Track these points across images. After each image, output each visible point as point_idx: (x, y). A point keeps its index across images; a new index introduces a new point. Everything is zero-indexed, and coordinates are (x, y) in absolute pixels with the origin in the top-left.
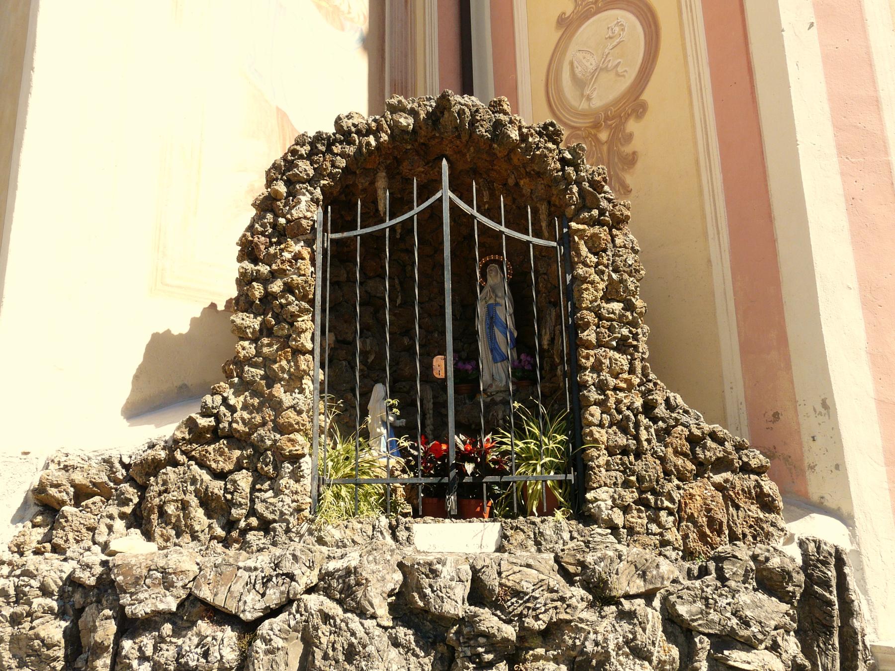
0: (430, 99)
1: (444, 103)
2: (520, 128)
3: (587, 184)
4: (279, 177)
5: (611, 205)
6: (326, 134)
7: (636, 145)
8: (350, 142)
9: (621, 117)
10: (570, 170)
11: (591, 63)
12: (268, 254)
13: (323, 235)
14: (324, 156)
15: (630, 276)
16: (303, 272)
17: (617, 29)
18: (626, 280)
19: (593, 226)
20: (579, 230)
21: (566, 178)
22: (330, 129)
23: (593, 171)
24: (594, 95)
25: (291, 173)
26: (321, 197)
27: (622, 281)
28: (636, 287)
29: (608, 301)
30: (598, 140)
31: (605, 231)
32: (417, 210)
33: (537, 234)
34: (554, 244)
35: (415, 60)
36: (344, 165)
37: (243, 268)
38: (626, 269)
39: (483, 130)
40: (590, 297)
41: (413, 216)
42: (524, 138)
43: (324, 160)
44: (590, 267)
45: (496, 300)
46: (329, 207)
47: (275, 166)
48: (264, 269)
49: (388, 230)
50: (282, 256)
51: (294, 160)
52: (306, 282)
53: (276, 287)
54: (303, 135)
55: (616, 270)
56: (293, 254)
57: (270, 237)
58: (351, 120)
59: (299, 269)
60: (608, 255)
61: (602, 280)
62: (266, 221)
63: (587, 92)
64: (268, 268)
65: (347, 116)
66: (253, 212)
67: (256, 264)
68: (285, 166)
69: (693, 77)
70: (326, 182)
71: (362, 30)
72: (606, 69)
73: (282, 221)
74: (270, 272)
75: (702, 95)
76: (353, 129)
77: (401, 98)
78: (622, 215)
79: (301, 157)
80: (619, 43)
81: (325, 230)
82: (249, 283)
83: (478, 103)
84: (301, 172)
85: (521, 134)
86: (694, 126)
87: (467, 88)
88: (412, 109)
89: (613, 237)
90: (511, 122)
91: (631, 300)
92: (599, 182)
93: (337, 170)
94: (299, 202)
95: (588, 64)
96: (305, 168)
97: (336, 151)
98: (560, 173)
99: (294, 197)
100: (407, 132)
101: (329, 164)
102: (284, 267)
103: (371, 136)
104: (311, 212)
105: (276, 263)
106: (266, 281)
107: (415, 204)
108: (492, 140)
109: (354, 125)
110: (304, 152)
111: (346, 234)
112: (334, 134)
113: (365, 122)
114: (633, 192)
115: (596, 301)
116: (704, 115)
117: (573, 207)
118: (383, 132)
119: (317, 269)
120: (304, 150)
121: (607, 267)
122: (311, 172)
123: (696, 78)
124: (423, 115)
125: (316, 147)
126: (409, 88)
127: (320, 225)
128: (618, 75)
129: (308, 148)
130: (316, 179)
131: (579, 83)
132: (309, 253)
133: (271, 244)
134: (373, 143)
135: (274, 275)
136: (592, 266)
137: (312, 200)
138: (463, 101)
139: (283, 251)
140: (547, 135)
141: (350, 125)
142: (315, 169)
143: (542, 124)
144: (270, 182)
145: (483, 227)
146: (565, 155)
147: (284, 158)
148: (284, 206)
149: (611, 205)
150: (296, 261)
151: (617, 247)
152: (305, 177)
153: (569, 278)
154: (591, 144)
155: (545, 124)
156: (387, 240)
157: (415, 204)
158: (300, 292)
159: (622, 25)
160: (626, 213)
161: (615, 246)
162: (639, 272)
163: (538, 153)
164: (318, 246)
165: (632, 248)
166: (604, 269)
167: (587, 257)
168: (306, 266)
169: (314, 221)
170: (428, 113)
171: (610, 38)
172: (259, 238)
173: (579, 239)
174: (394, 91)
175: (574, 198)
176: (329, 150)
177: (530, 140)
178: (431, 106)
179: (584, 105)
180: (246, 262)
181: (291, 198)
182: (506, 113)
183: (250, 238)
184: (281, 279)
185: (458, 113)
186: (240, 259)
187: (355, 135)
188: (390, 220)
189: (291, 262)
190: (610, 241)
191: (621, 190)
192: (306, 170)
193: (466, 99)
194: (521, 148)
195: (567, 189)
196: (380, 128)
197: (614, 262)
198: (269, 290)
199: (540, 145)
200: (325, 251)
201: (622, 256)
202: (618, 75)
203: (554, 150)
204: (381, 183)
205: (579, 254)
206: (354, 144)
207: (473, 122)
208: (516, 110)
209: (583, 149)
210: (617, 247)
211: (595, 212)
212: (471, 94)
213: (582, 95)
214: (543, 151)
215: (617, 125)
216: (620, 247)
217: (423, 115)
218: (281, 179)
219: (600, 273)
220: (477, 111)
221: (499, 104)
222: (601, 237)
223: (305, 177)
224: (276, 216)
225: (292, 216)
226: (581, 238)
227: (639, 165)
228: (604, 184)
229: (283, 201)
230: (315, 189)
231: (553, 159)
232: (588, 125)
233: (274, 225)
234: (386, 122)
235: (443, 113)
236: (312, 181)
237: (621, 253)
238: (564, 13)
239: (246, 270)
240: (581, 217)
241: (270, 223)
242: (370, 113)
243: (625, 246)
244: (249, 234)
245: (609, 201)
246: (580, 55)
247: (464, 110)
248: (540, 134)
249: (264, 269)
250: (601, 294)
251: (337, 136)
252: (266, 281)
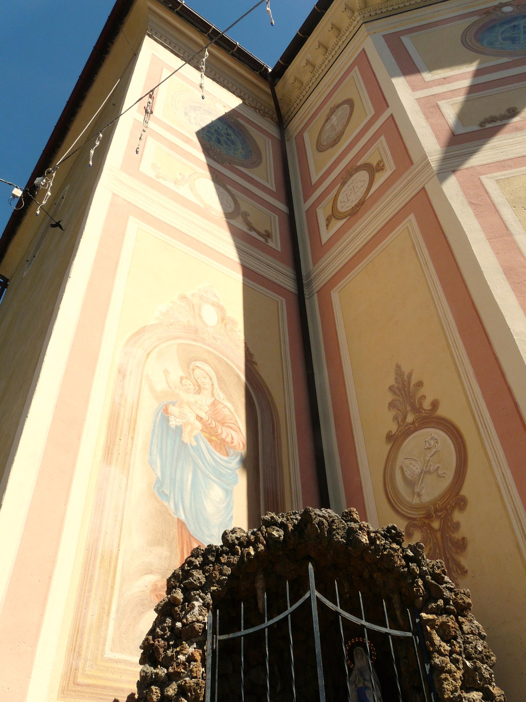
0: (296, 513)
1: (306, 516)
2: (368, 533)
3: (430, 577)
4: (178, 584)
5: (453, 594)
6: (216, 546)
7: (463, 532)
8: (234, 553)
9: (447, 510)
10: (413, 565)
11: (416, 468)
12: (166, 656)
13: (213, 637)
14: (214, 566)
15: (483, 663)
16: (195, 675)
17: (432, 442)
18: (480, 668)
19: (441, 614)
20: (429, 620)
21: (411, 572)
22: (218, 543)
23: (433, 565)
24: (423, 492)
25: (186, 581)
26: (211, 602)
27: (476, 669)
28: (490, 675)
29: (468, 691)
30: (431, 528)
31: (452, 619)
32: (290, 609)
33: (395, 626)
34: (410, 634)
35: (282, 467)
36: (230, 572)
37: (144, 671)
38: (478, 656)
39: (339, 537)
40: (450, 687)
41: (287, 616)
42: (372, 541)
43: (214, 570)
44: (444, 655)
45: (364, 684)
46: (218, 611)
47: (174, 575)
48: (162, 671)
49: (266, 630)
50: (178, 659)
51: (189, 570)
52: (197, 684)
53: (171, 690)
54: (197, 548)
55: (469, 658)
56: (187, 656)
57: (167, 640)
58: (235, 535)
59: (191, 671)
60: (459, 643)
61: (459, 669)
62: (165, 625)
63: (417, 490)
64: (166, 671)
65: (231, 531)
66: (154, 615)
67: (155, 667)
68: (182, 575)
69: (499, 477)
70: (216, 588)
71: (241, 454)
72: (429, 472)
73: (179, 625)
74: (167, 674)
75: (509, 490)
76: (237, 542)
77: (273, 515)
78: (464, 602)
79: (196, 567)
80: (436, 452)
81: (214, 633)
82: (148, 686)
83: (333, 514)
84: (195, 581)
85: (370, 538)
86: (508, 516)
87: (325, 503)
88: (282, 523)
89: (460, 624)
90: (361, 528)
91: (488, 688)
92: (439, 574)
93: (224, 577)
94: (193, 607)
95: (414, 469)
96: (198, 576)
97: (223, 561)
98: (406, 569)
99: (189, 602)
100: (280, 542)
101: (217, 573)
102: (179, 670)
103: (251, 547)
104: (203, 616)
105: (172, 665)
106: (163, 683)
107: (289, 604)
108: (347, 544)
109: (237, 538)
110: (197, 563)
111: (231, 636)
112: (221, 546)
113: (245, 535)
114: (469, 572)
115: (456, 691)
116: (515, 506)
117: (421, 598)
118: (260, 543)
119: (207, 670)
120: (197, 562)
121: (460, 654)
122: (203, 580)
123: (501, 478)
124: (291, 528)
125: (208, 558)
126: (279, 494)
127: (210, 627)
128: (439, 476)
129: (201, 559)
130: (208, 586)
131: (410, 483)
132: (200, 654)
133: (169, 647)
134: (253, 553)
135: (171, 678)
136: (447, 655)
137: (204, 604)
138: (321, 514)
139: (179, 654)
140: (391, 537)
141: (234, 538)
142: (206, 577)
143: (385, 527)
144: (170, 589)
145: (346, 621)
146: (407, 553)
147: (182, 568)
148: (181, 611)
149: (453, 594)
150: (190, 664)
151: (465, 634)
152: (198, 585)
153: (427, 667)
154: (427, 532)
155: (388, 528)
156: (266, 639)
157: (289, 604)
158: (191, 694)
159: (436, 439)
160: (469, 601)
161: (463, 633)
162: (490, 658)
163: (385, 553)
164: (208, 647)
165: (479, 634)
166: (458, 657)
167: (440, 646)
168: (198, 669)
169: (205, 624)
170: (294, 526)
171: (428, 448)
172: (159, 642)
173: (431, 628)
174: (267, 509)
175: (421, 591)
176: (218, 560)
177: (378, 542)
178: (296, 519)
179: (416, 501)
180: (147, 666)
181: (187, 603)
182: (355, 521)
183: (152, 642)
184: (176, 682)
185: (318, 524)
186: (142, 662)
187: (238, 547)
188: (268, 621)
189: (185, 665)
190: (458, 628)
191: (459, 571)
192: (199, 579)
193: (324, 511)
194: (371, 550)
195: (413, 582)
196: (257, 540)
197: (465, 649)
198: (166, 693)
199: (387, 546)
200: (214, 652)
201: (472, 643)
202: (439, 476)
203: (398, 549)
204: (260, 584)
205: (433, 644)
206: (238, 555)
207: (331, 530)
208: (364, 517)
209: (421, 547)
210: (465, 634)
211: (441, 602)
212: (328, 507)
213: (413, 492)
214: (389, 551)
215: (445, 516)
216: (468, 634)
217: (291, 528)
218: (179, 587)
219: (455, 662)
220: (333, 521)
221: (350, 513)
222: (449, 626)
223: (198, 585)
224: (174, 621)
225: (187, 621)
226: (432, 628)
227: (470, 548)
228: (443, 576)
229: (180, 606)
230: (206, 594)
231: (398, 557)
232: (422, 516)
233: (173, 628)
234: (262, 534)
235: (306, 525)
236: (204, 588)
237: (470, 640)
238: (391, 432)
239: (146, 673)
240: (429, 607)
241: (169, 627)
242: (250, 527)
243: (472, 633)
244: (150, 637)
245: (451, 590)
246: (407, 462)
247: (323, 521)
248: (384, 536)
249: (162, 671)
250: (459, 683)
251: (224, 548)
252: (163, 683)
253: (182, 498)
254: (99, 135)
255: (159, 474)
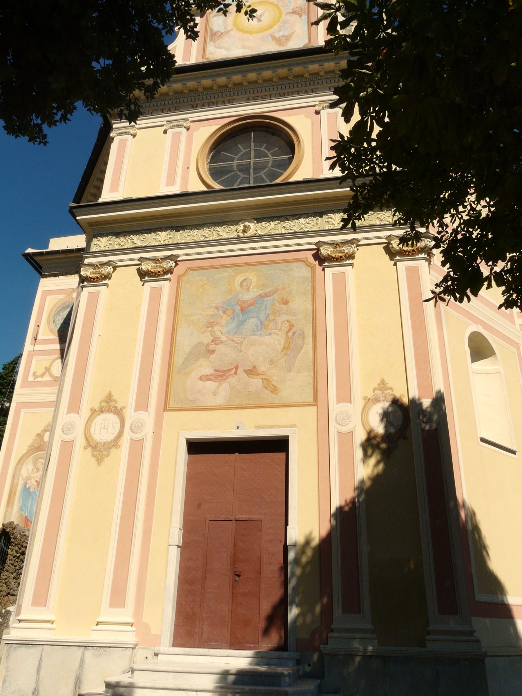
253: (27, 510)
254: (428, 430)
255: (21, 504)
